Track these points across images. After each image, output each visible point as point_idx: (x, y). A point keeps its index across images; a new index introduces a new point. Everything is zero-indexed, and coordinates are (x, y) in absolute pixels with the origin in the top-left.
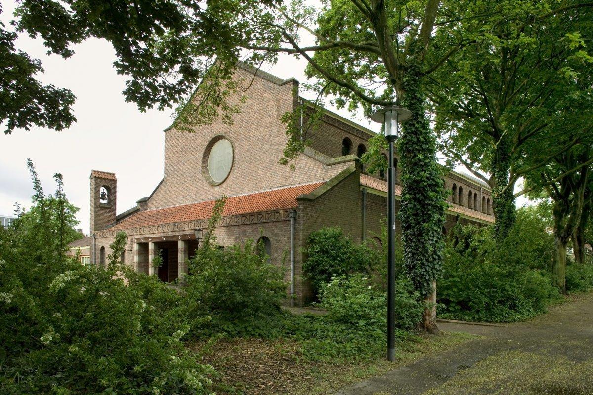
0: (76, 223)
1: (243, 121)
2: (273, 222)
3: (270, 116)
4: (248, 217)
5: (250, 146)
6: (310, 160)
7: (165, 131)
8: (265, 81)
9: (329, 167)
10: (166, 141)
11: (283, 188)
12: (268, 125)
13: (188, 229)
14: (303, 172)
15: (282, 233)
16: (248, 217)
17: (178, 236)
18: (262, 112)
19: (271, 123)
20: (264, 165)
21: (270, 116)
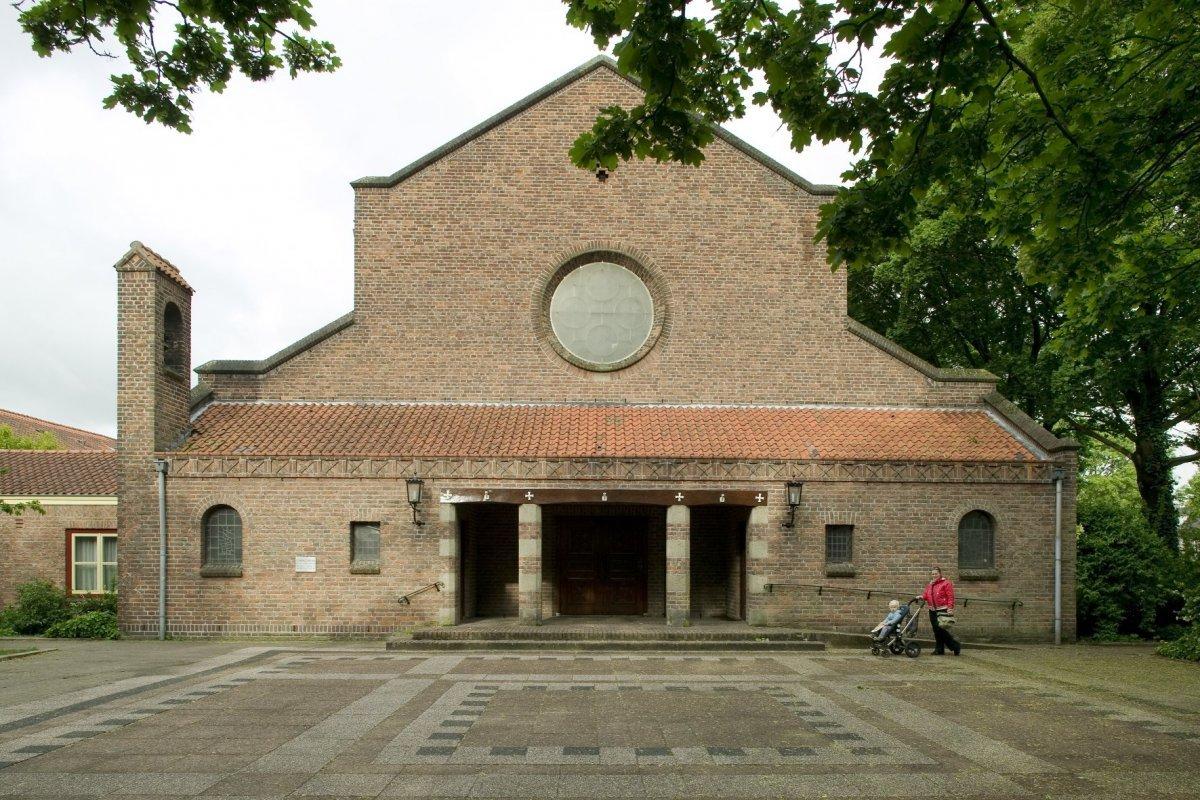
0: (273, 48)
1: (693, 237)
2: (1004, 484)
3: (781, 247)
4: (958, 466)
5: (720, 300)
6: (895, 362)
7: (356, 186)
8: (765, 169)
9: (940, 384)
10: (121, 285)
11: (820, 407)
12: (778, 266)
13: (691, 477)
14: (877, 382)
15: (1028, 506)
16: (958, 466)
17: (526, 491)
18: (759, 235)
19: (786, 266)
20: (766, 350)
21: (781, 247)
